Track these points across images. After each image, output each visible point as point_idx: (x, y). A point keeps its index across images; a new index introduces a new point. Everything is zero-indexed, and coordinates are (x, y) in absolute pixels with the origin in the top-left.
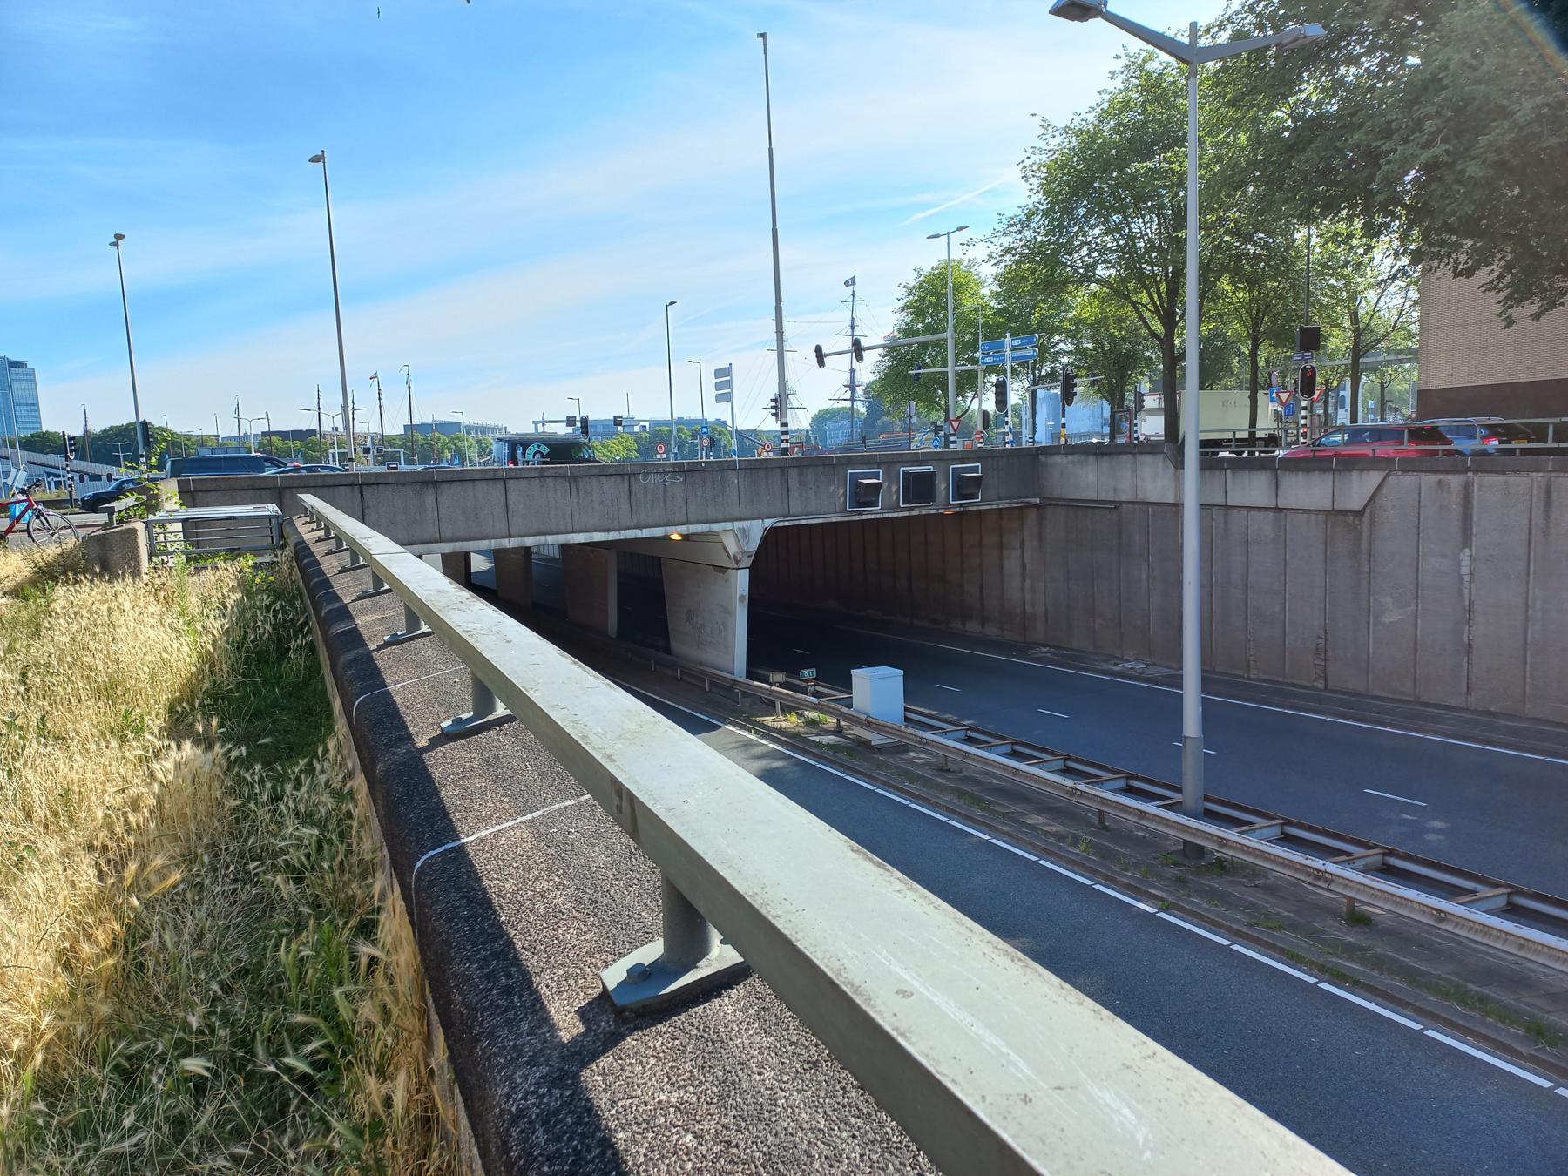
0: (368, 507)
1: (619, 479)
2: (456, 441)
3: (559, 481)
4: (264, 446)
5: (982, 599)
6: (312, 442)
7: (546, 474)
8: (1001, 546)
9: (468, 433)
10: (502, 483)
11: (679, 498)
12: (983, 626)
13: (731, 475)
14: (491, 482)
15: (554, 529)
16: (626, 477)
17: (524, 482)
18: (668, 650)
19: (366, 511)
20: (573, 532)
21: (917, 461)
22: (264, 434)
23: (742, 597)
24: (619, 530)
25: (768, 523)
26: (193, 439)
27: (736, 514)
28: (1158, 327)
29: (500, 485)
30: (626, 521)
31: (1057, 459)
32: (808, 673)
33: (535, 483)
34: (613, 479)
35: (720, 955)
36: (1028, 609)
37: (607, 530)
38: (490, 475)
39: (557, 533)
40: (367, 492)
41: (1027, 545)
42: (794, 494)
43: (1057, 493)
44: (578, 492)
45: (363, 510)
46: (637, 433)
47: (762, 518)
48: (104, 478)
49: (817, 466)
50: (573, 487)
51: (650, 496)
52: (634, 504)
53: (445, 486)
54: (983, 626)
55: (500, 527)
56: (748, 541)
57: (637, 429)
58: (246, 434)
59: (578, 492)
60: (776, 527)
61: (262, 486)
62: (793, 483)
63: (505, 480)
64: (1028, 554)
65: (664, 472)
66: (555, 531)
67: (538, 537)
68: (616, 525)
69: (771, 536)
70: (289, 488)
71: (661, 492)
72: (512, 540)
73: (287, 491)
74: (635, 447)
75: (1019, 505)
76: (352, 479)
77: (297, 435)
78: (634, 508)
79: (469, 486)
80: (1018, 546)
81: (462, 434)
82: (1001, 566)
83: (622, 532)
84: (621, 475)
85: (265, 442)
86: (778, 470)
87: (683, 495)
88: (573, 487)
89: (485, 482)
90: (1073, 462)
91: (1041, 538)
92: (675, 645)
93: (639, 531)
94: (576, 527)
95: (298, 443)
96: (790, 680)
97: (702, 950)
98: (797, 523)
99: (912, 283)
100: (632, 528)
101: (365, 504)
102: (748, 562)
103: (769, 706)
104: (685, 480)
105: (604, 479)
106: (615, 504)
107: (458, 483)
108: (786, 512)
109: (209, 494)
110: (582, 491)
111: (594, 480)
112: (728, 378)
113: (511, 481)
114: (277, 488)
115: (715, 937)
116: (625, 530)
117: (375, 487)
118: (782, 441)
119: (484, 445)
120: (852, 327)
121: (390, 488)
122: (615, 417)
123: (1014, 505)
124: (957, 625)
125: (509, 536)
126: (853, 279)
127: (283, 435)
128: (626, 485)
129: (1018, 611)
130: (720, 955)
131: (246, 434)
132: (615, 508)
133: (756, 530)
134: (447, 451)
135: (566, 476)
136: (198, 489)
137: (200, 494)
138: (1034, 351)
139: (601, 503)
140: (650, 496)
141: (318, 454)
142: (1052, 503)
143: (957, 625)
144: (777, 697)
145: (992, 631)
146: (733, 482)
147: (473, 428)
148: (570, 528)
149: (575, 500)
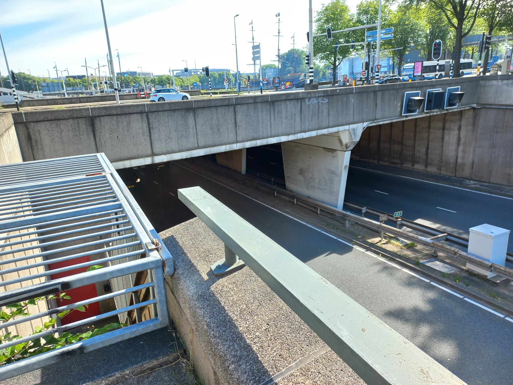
0: (153, 128)
1: (296, 102)
2: (135, 78)
3: (264, 104)
4: (67, 81)
5: (427, 153)
6: (84, 80)
7: (258, 100)
8: (444, 129)
9: (139, 75)
10: (233, 107)
11: (325, 113)
12: (426, 167)
13: (351, 96)
14: (227, 107)
15: (126, 99)
16: (299, 101)
17: (245, 106)
18: (284, 186)
19: (152, 131)
20: (271, 137)
21: (432, 86)
22: (67, 77)
23: (346, 166)
24: (295, 134)
25: (366, 124)
26: (41, 79)
27: (351, 120)
28: (455, 21)
29: (231, 109)
30: (298, 129)
31: (494, 82)
32: (398, 214)
33: (252, 106)
34: (293, 102)
35: (239, 262)
36: (459, 161)
37: (288, 135)
38: (226, 103)
39: (263, 138)
40: (152, 117)
41: (463, 128)
42: (379, 107)
43: (491, 101)
44: (274, 111)
45: (149, 130)
46: (199, 75)
47: (363, 122)
48: (9, 94)
49: (389, 90)
50: (272, 109)
51: (311, 112)
52: (303, 118)
53: (200, 111)
54: (426, 167)
55: (232, 137)
56: (356, 136)
57: (199, 73)
58: (60, 77)
59: (274, 111)
60: (370, 127)
61: (79, 116)
62: (379, 101)
63: (234, 106)
64: (463, 134)
65: (319, 97)
66: (261, 137)
67: (252, 142)
68: (293, 132)
69: (367, 132)
70: (98, 116)
71: (317, 108)
72: (238, 144)
73: (97, 119)
74: (199, 80)
75: (468, 108)
76: (141, 108)
77: (80, 77)
78: (303, 120)
79: (214, 110)
80: (456, 128)
81: (137, 76)
82: (443, 139)
83: (296, 135)
84: (297, 99)
85: (67, 80)
86: (373, 93)
87: (327, 110)
88: (272, 109)
89: (224, 107)
90: (507, 85)
91: (474, 124)
92: (290, 185)
93: (304, 134)
94: (273, 134)
95: (79, 80)
96: (369, 211)
97: (234, 261)
98: (378, 124)
99: (320, 10)
100: (301, 132)
101: (151, 126)
102: (352, 147)
103: (376, 232)
104: (329, 101)
105: (288, 102)
106: (293, 118)
107: (208, 109)
108: (374, 118)
109: (39, 124)
110: (276, 110)
111: (283, 104)
112: (259, 49)
113: (238, 106)
114: (89, 117)
115: (237, 257)
116: (297, 133)
117: (156, 113)
118: (312, 76)
119: (146, 80)
120: (279, 33)
121: (166, 114)
122: (185, 68)
123: (467, 108)
124: (408, 165)
125: (237, 142)
126: (279, 15)
127: (74, 77)
128: (299, 105)
129: (452, 161)
130: (239, 262)
131: (60, 77)
132: (293, 121)
133: (360, 128)
134: (132, 82)
135: (268, 102)
136: (30, 120)
137: (32, 124)
138: (392, 35)
139: (286, 118)
140: (311, 112)
141: (87, 84)
142: (487, 107)
143: (408, 165)
144: (383, 229)
145: (432, 169)
146: (351, 101)
147: (141, 73)
148: (269, 135)
149: (272, 117)
